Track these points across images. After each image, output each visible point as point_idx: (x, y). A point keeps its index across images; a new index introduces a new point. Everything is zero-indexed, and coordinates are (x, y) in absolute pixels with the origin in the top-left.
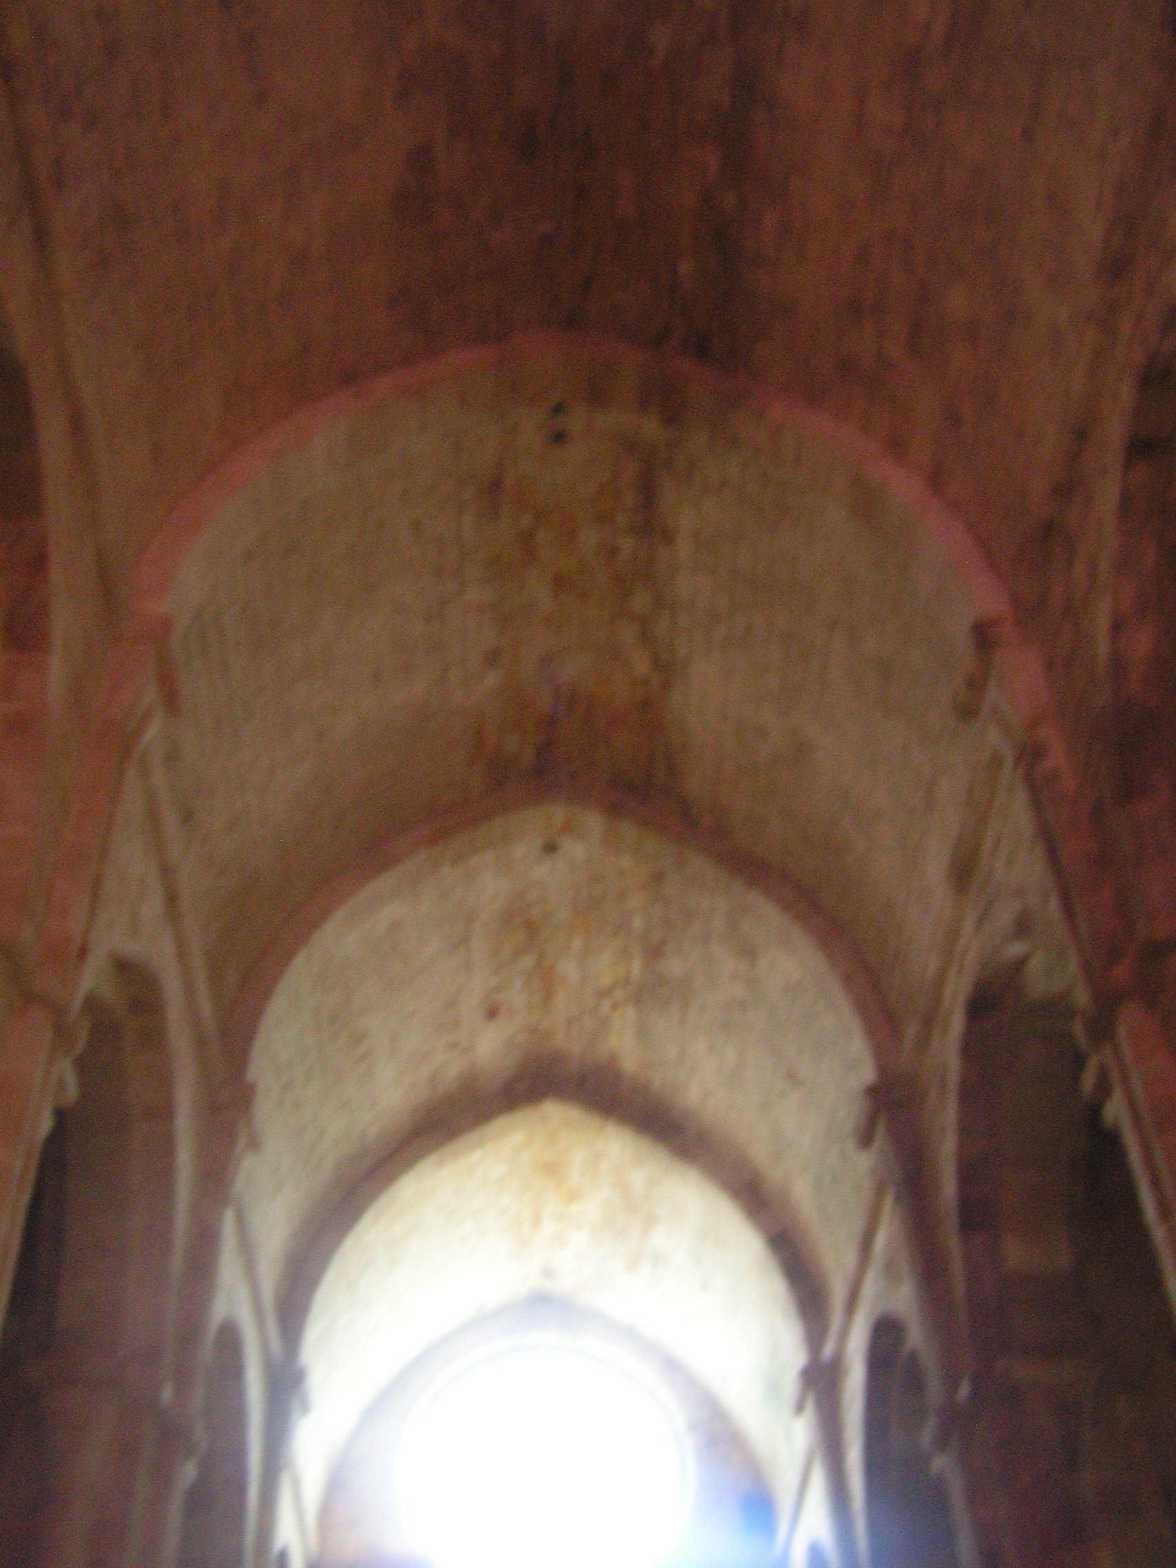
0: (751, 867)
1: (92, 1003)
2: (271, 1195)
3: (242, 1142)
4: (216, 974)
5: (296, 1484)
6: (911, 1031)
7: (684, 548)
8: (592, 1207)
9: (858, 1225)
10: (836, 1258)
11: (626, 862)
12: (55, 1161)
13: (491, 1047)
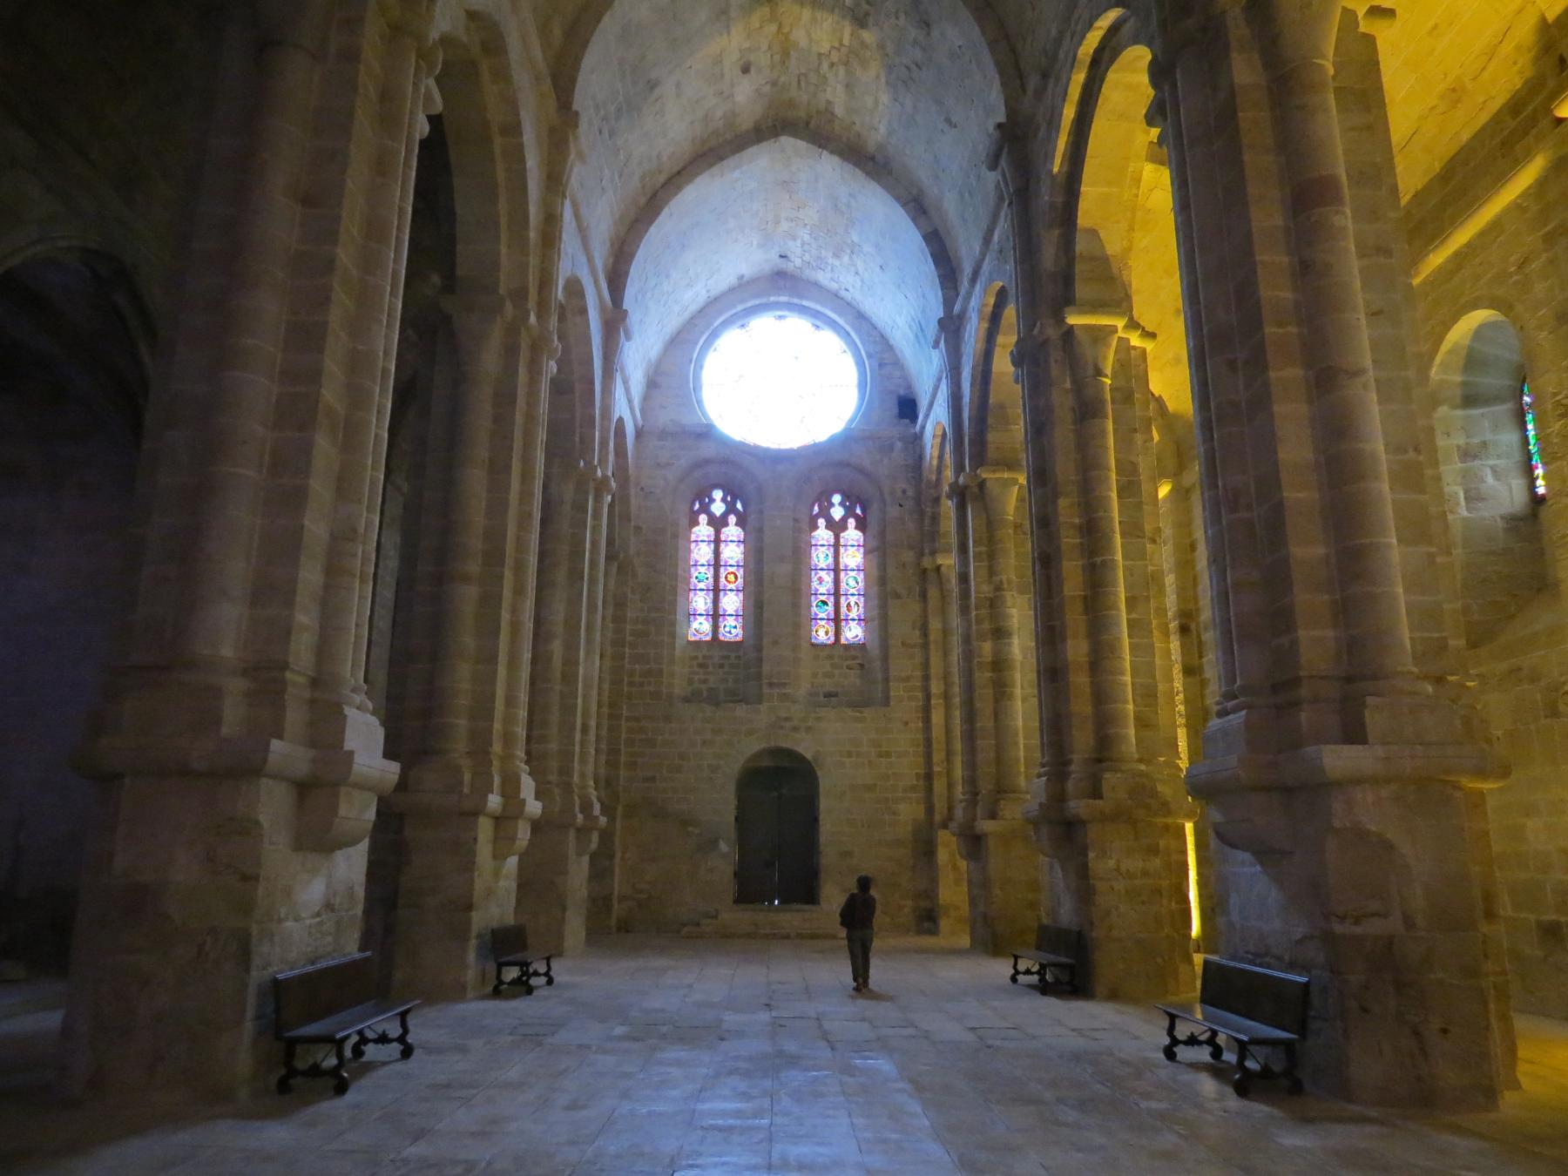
1: (446, 41)
4: (544, 30)
5: (626, 382)
6: (1033, 81)
9: (984, 225)
10: (967, 246)
12: (434, 151)
13: (746, 97)
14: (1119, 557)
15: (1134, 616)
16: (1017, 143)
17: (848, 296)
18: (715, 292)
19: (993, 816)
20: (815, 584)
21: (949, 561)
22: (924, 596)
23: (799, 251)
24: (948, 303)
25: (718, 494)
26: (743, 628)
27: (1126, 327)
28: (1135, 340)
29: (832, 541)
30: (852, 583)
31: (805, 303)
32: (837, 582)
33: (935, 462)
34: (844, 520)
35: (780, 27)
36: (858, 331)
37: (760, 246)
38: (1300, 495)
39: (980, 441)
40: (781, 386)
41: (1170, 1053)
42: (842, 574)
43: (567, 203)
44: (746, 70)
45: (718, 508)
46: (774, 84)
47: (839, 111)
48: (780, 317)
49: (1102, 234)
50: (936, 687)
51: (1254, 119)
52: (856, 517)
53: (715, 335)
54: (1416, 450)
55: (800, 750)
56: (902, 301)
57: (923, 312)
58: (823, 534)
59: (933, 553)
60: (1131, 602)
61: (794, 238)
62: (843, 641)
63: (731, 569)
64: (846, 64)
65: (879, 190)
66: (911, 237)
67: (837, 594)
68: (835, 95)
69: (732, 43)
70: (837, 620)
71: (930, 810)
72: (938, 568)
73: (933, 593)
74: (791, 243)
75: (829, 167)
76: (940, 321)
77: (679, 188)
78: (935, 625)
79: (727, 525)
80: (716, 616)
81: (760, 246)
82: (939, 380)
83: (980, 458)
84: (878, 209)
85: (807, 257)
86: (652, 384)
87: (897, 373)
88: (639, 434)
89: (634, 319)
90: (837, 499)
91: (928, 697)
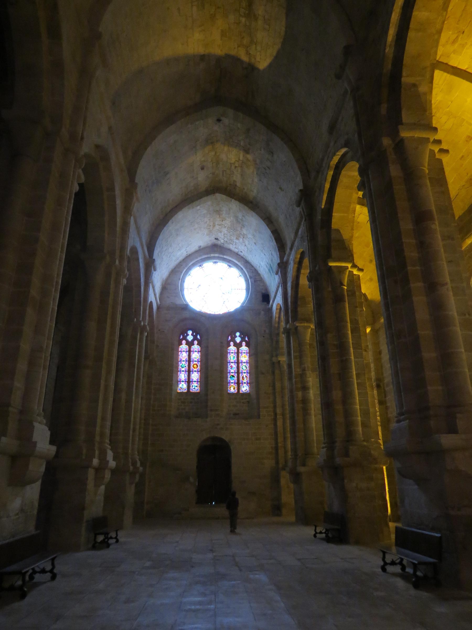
0: (273, 127)
2: (142, 219)
3: (135, 199)
5: (153, 287)
7: (260, 22)
8: (228, 222)
10: (288, 235)
11: (239, 125)
12: (80, 198)
13: (202, 179)
14: (353, 358)
15: (359, 381)
16: (307, 197)
17: (242, 254)
18: (189, 253)
19: (304, 465)
20: (229, 368)
21: (283, 359)
22: (273, 373)
23: (222, 237)
24: (281, 257)
25: (190, 332)
26: (200, 387)
27: (352, 267)
28: (355, 272)
29: (236, 351)
30: (244, 368)
31: (225, 257)
32: (238, 368)
33: (277, 319)
34: (241, 343)
35: (216, 153)
36: (246, 268)
37: (207, 235)
38: (425, 332)
39: (295, 311)
40: (215, 290)
41: (384, 569)
42: (240, 364)
43: (132, 218)
44: (202, 168)
45: (190, 338)
46: (213, 174)
47: (238, 184)
48: (215, 262)
49: (341, 231)
50: (279, 411)
51: (399, 189)
52: (246, 341)
53: (190, 269)
54: (469, 315)
55: (224, 437)
56: (263, 257)
57: (272, 260)
58: (232, 348)
59: (277, 356)
60: (358, 375)
61: (221, 232)
62: (241, 392)
63: (195, 363)
64: (241, 167)
65: (254, 214)
66: (267, 232)
67: (238, 373)
68: (237, 178)
69: (198, 158)
70: (238, 384)
71: (277, 463)
72: (279, 362)
73: (277, 372)
74: (219, 234)
75: (234, 205)
76: (279, 264)
77: (176, 213)
78: (278, 385)
79: (193, 345)
80: (189, 382)
81: (207, 235)
82: (278, 287)
83: (295, 318)
84: (253, 221)
85: (226, 239)
86: (164, 288)
87: (261, 284)
88: (158, 308)
89: (157, 263)
90: (238, 334)
91: (276, 414)
